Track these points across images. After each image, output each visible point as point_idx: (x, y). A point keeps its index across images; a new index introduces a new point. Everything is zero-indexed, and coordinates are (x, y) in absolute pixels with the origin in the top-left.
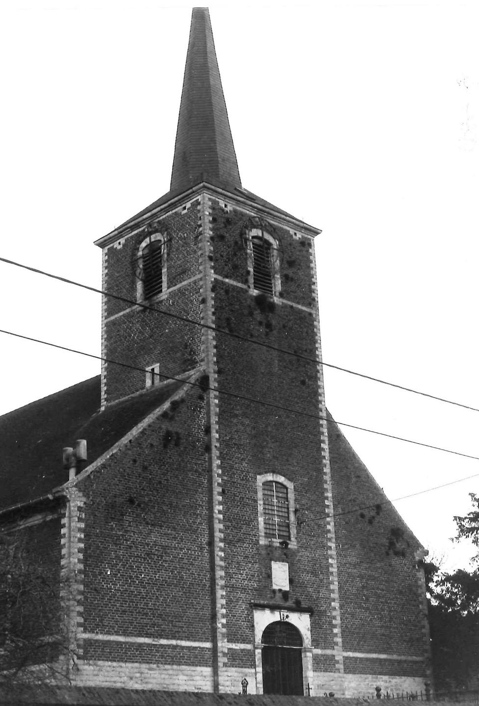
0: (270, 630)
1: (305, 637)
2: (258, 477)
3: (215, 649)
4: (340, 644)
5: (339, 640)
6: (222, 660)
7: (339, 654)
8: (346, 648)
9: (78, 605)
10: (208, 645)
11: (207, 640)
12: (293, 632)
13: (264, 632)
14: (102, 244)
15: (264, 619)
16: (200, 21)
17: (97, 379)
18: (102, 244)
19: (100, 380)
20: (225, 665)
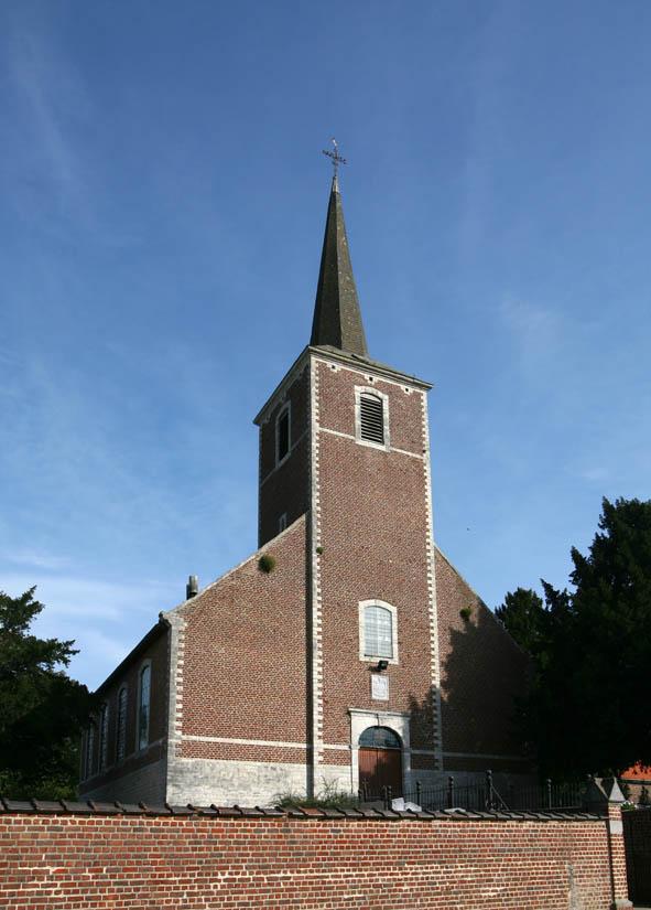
7: (438, 754)
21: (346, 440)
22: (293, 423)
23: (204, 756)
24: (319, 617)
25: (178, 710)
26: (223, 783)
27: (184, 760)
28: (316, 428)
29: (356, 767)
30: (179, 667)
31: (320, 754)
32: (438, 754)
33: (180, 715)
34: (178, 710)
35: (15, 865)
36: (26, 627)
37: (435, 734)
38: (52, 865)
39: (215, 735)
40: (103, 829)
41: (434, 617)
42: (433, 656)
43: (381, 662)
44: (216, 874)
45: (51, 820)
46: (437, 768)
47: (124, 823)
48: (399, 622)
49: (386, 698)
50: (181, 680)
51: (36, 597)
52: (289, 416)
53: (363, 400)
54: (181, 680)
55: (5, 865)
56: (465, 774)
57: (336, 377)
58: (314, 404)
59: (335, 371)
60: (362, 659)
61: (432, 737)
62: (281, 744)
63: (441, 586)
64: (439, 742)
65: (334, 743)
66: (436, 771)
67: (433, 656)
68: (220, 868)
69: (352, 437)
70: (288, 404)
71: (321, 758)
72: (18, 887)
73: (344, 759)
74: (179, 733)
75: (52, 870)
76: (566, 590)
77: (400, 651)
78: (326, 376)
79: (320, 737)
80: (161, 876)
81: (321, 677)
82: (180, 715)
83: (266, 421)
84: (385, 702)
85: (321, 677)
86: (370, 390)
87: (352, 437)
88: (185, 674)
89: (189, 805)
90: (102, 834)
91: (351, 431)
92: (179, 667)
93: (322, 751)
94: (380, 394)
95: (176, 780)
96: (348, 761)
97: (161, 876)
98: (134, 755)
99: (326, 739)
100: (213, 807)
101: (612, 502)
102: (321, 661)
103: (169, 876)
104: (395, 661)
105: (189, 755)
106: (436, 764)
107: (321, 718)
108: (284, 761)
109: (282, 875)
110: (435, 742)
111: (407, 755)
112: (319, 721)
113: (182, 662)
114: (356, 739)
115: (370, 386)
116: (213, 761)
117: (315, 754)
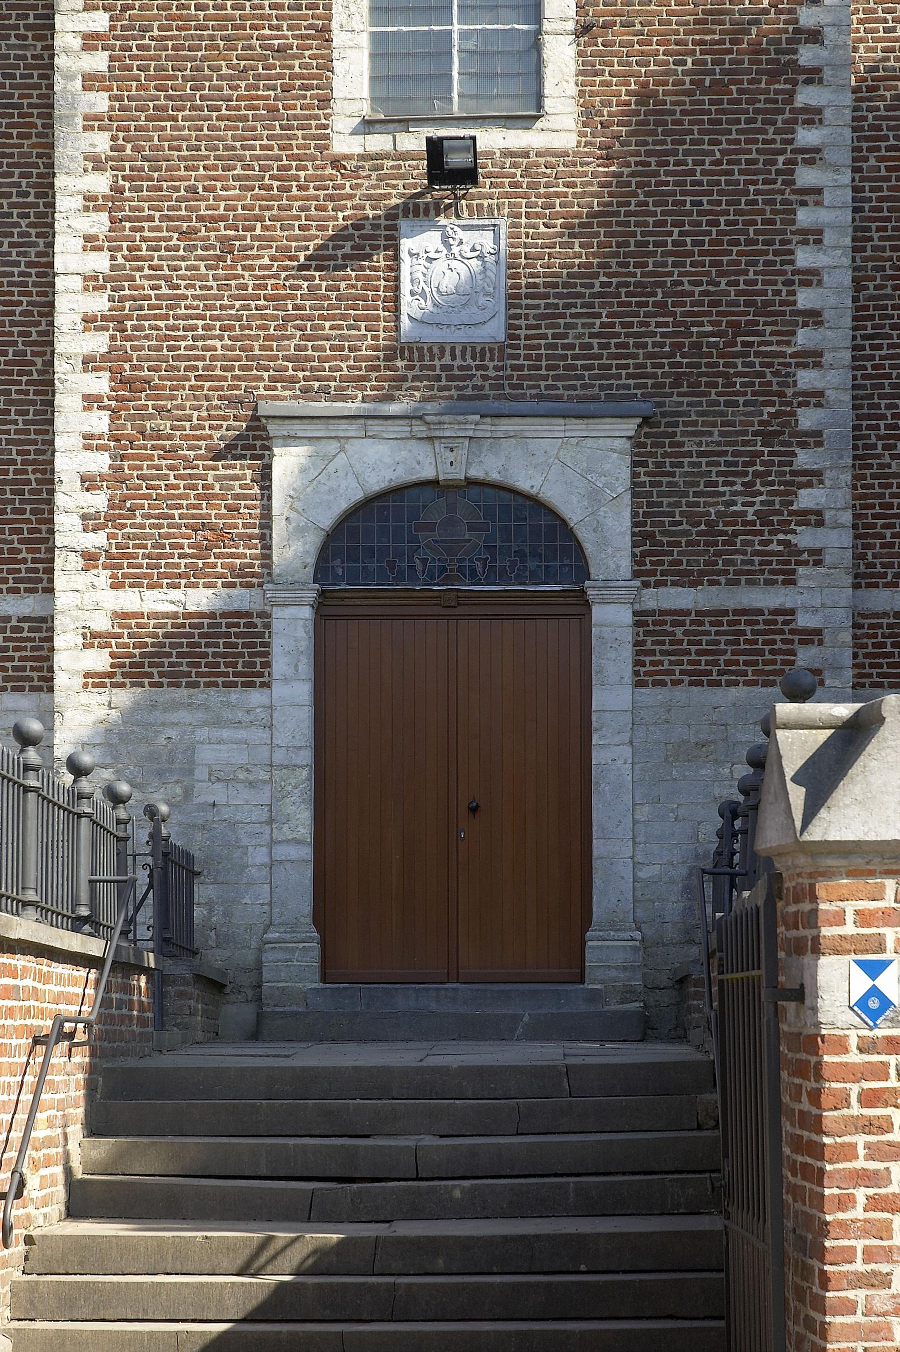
55: (892, 367)
60: (345, 143)
61: (781, 517)
64: (836, 541)
77: (586, 71)
79: (89, 558)
81: (100, 262)
85: (100, 262)
90: (304, 12)
93: (102, 623)
96: (253, 670)
110: (805, 538)
112: (89, 482)
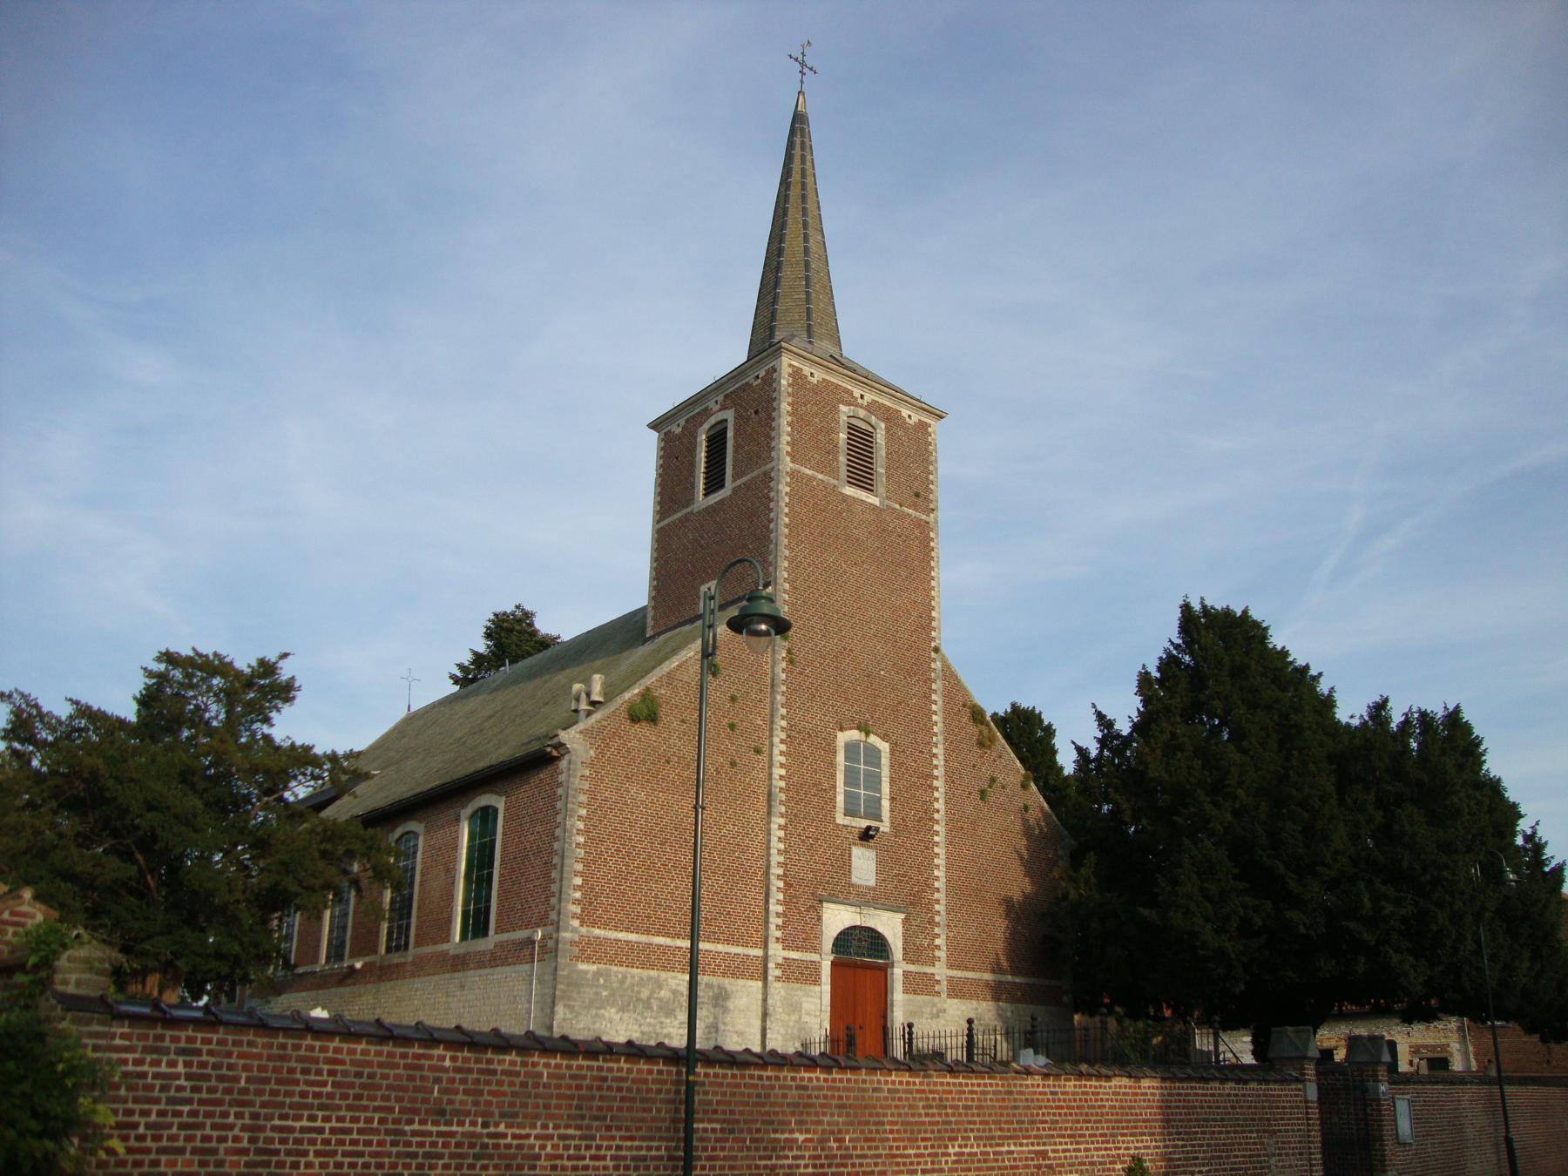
0: (845, 940)
1: (890, 939)
2: (840, 734)
3: (766, 958)
4: (944, 959)
5: (942, 954)
6: (774, 972)
7: (941, 971)
8: (951, 966)
9: (144, 983)
10: (759, 952)
11: (755, 945)
12: (875, 942)
13: (837, 939)
14: (654, 426)
15: (837, 918)
16: (799, 122)
17: (645, 608)
18: (654, 426)
19: (645, 617)
20: (778, 979)
21: (826, 486)
22: (737, 447)
23: (611, 962)
24: (782, 753)
25: (577, 888)
26: (630, 1001)
27: (582, 966)
28: (787, 464)
29: (826, 987)
30: (580, 818)
31: (778, 965)
32: (941, 971)
33: (578, 895)
34: (577, 888)
35: (767, 1131)
36: (267, 720)
37: (937, 942)
38: (801, 1132)
39: (627, 930)
40: (845, 1089)
41: (939, 762)
42: (937, 822)
43: (869, 828)
44: (946, 1147)
45: (152, 1033)
46: (938, 993)
47: (250, 1044)
48: (892, 766)
49: (872, 883)
50: (581, 839)
51: (286, 671)
52: (730, 434)
53: (850, 427)
54: (581, 839)
56: (974, 1003)
57: (816, 390)
58: (784, 423)
59: (814, 381)
62: (720, 948)
63: (949, 716)
65: (797, 949)
66: (936, 999)
67: (937, 822)
68: (950, 1139)
69: (833, 481)
70: (729, 415)
71: (778, 972)
72: (770, 1158)
73: (808, 974)
74: (576, 923)
75: (801, 1137)
76: (1103, 721)
77: (892, 811)
78: (802, 387)
80: (898, 1148)
82: (578, 895)
83: (677, 430)
84: (869, 888)
85: (782, 846)
86: (862, 413)
87: (833, 481)
88: (586, 832)
89: (378, 1021)
91: (834, 473)
92: (580, 818)
93: (780, 961)
94: (873, 419)
95: (570, 998)
96: (816, 981)
97: (898, 1148)
98: (445, 947)
99: (787, 943)
100: (630, 1043)
101: (1196, 606)
102: (782, 821)
103: (905, 1148)
104: (885, 827)
105: (588, 960)
106: (937, 988)
107: (780, 909)
108: (724, 975)
109: (1005, 1148)
111: (898, 972)
113: (583, 812)
114: (828, 944)
115: (861, 407)
116: (623, 969)
117: (771, 965)
